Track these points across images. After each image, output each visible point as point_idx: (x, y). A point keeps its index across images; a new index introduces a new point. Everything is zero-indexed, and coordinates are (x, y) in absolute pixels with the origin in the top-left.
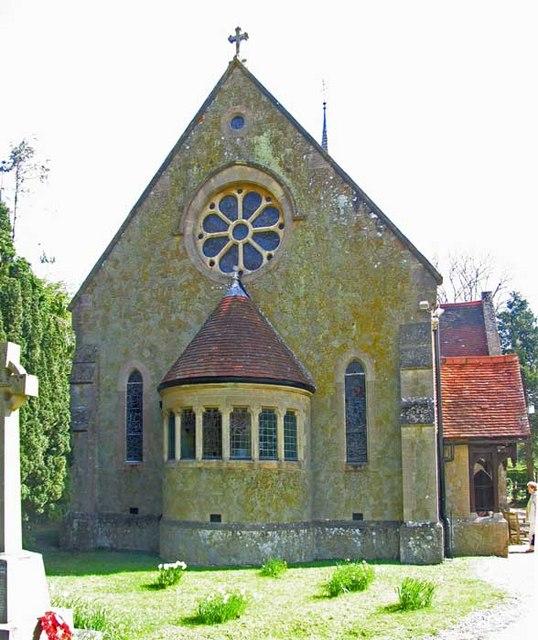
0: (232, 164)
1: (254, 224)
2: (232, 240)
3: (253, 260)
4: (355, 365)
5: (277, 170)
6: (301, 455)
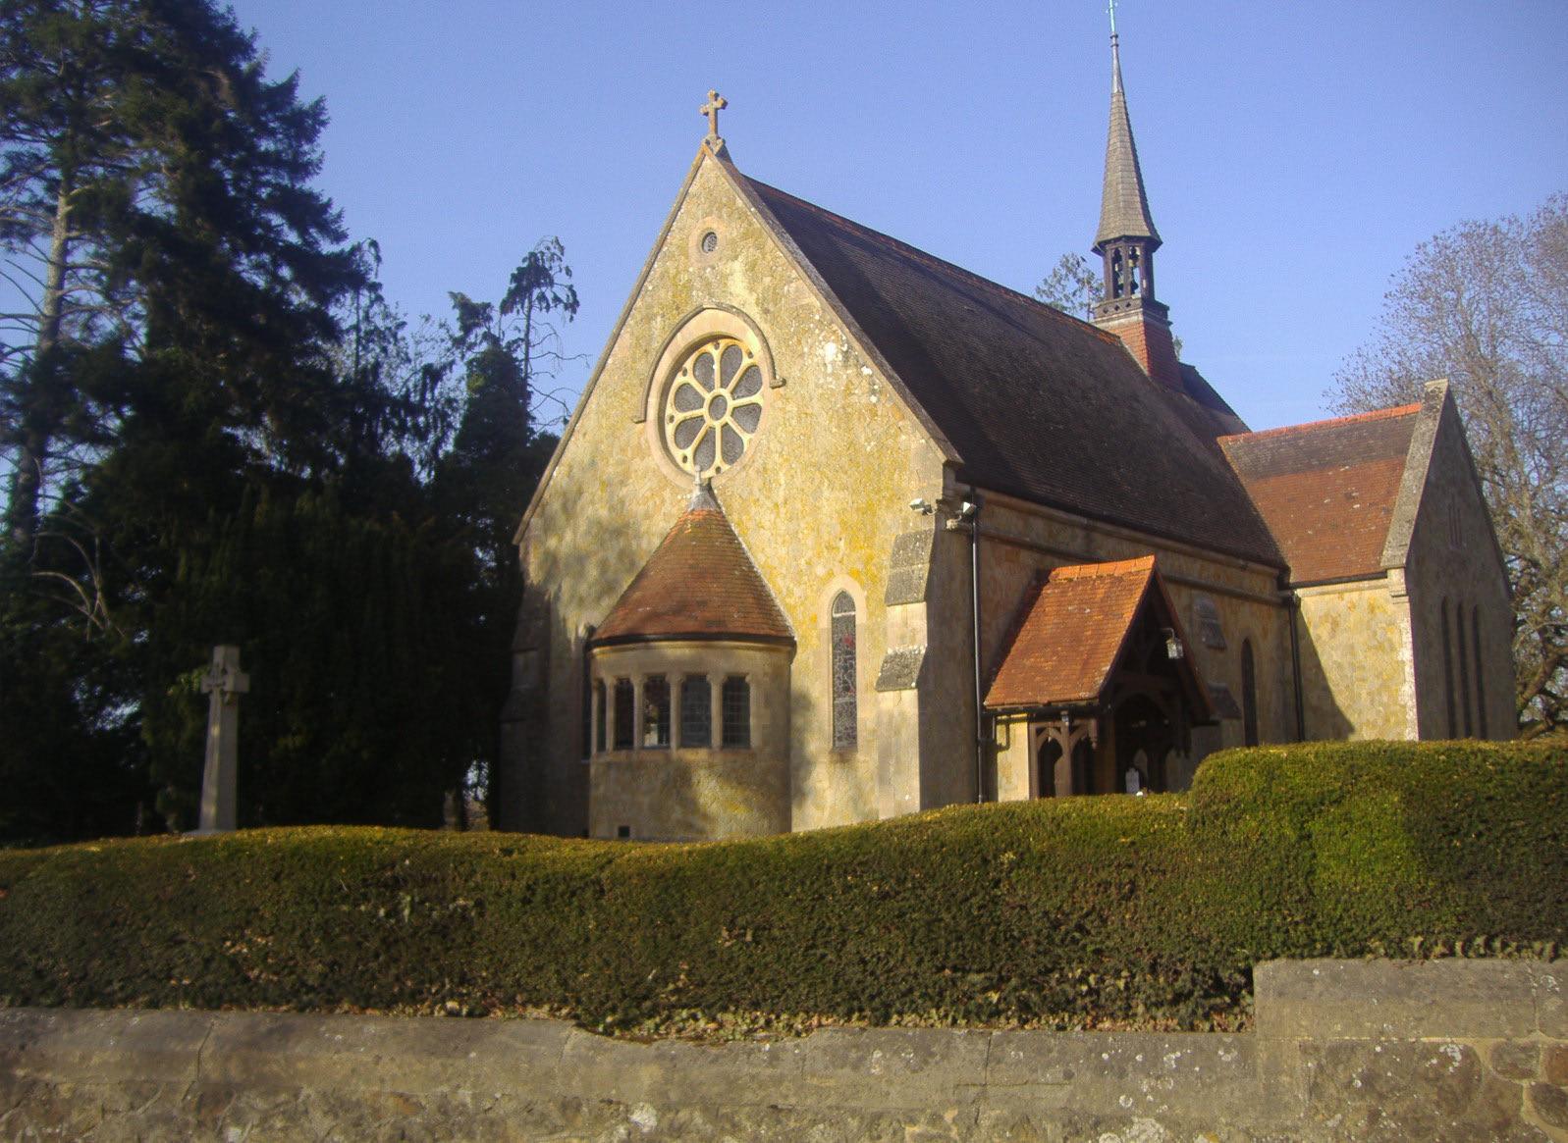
0: (700, 310)
1: (724, 385)
2: (727, 418)
3: (733, 450)
4: (843, 601)
5: (754, 312)
6: (755, 738)
